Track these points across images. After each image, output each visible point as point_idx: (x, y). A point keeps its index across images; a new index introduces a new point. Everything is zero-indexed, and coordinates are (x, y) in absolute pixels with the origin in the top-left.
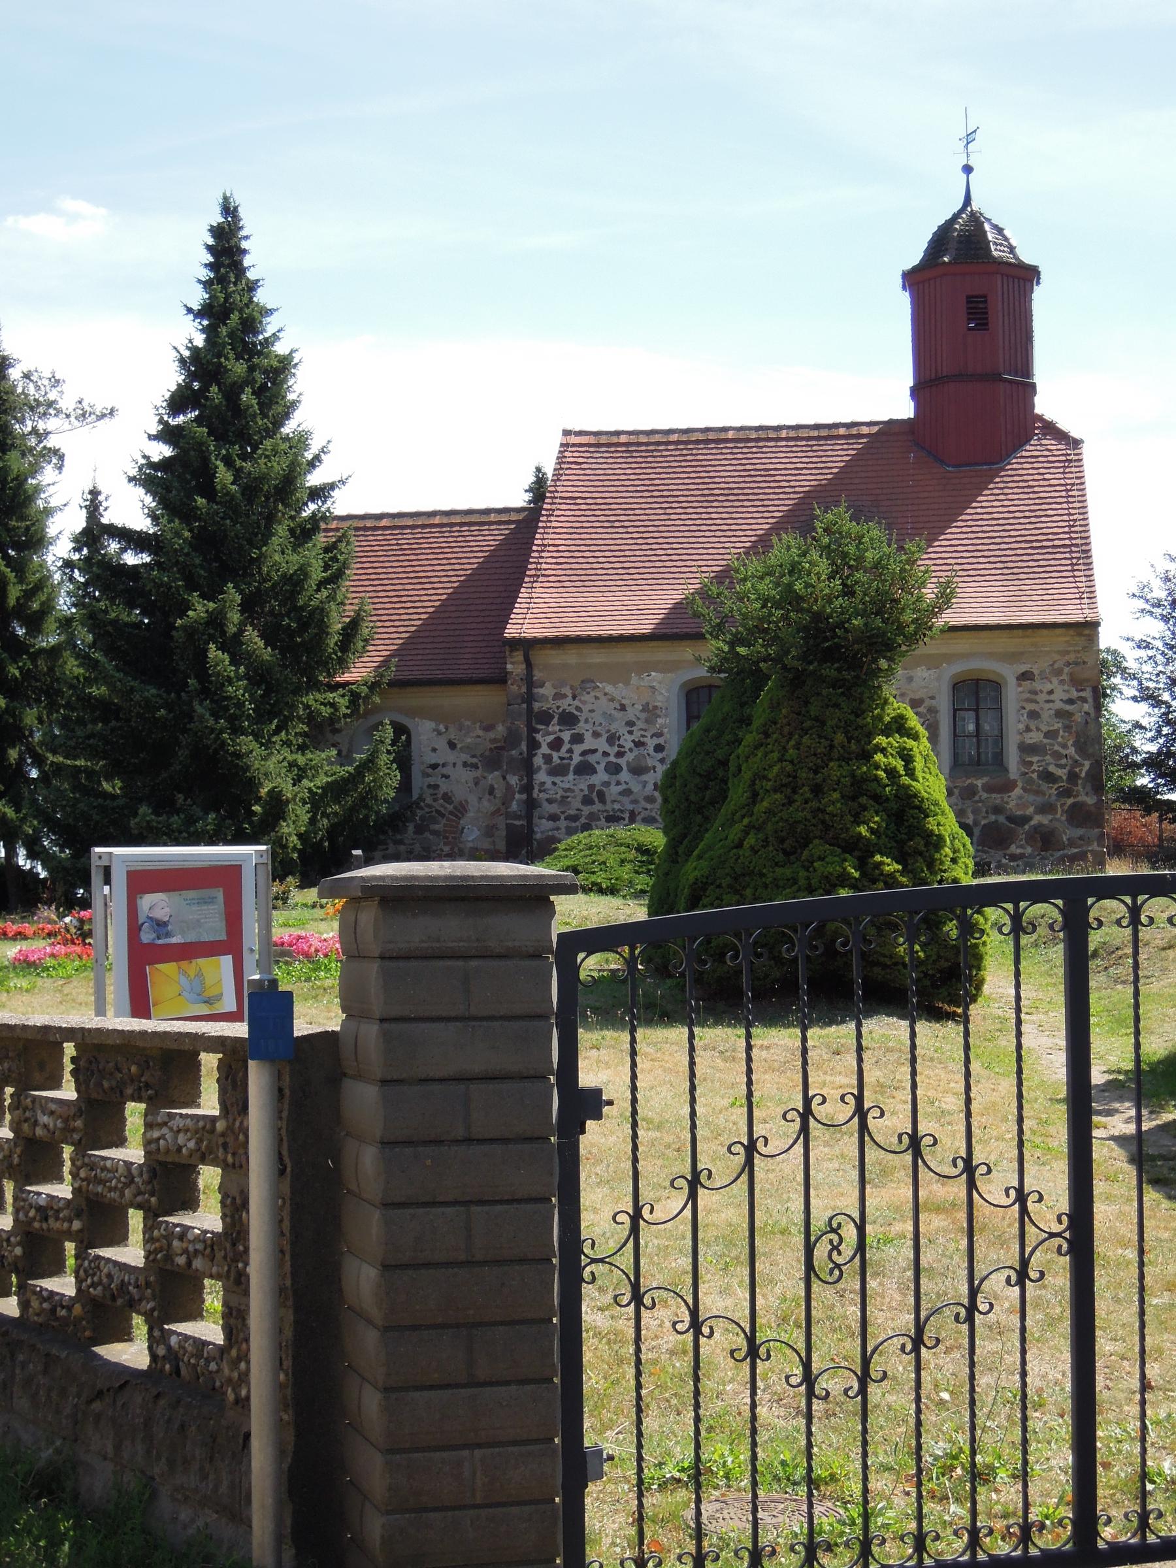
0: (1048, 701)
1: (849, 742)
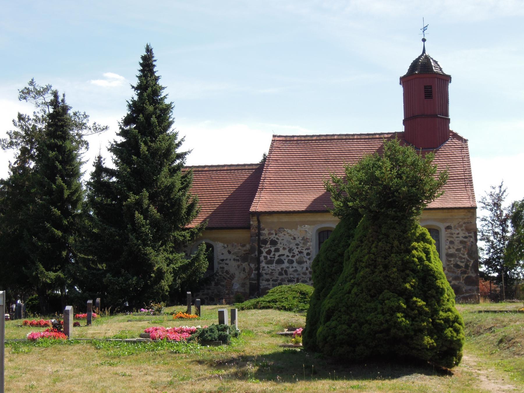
0: (457, 237)
1: (400, 245)
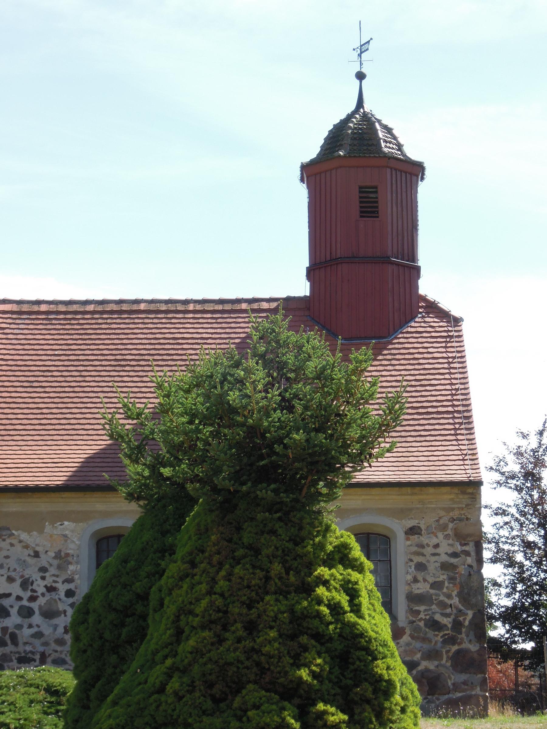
1: (287, 573)
